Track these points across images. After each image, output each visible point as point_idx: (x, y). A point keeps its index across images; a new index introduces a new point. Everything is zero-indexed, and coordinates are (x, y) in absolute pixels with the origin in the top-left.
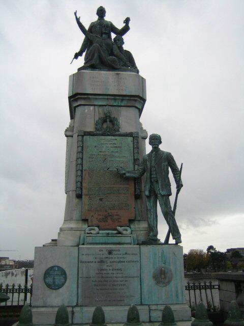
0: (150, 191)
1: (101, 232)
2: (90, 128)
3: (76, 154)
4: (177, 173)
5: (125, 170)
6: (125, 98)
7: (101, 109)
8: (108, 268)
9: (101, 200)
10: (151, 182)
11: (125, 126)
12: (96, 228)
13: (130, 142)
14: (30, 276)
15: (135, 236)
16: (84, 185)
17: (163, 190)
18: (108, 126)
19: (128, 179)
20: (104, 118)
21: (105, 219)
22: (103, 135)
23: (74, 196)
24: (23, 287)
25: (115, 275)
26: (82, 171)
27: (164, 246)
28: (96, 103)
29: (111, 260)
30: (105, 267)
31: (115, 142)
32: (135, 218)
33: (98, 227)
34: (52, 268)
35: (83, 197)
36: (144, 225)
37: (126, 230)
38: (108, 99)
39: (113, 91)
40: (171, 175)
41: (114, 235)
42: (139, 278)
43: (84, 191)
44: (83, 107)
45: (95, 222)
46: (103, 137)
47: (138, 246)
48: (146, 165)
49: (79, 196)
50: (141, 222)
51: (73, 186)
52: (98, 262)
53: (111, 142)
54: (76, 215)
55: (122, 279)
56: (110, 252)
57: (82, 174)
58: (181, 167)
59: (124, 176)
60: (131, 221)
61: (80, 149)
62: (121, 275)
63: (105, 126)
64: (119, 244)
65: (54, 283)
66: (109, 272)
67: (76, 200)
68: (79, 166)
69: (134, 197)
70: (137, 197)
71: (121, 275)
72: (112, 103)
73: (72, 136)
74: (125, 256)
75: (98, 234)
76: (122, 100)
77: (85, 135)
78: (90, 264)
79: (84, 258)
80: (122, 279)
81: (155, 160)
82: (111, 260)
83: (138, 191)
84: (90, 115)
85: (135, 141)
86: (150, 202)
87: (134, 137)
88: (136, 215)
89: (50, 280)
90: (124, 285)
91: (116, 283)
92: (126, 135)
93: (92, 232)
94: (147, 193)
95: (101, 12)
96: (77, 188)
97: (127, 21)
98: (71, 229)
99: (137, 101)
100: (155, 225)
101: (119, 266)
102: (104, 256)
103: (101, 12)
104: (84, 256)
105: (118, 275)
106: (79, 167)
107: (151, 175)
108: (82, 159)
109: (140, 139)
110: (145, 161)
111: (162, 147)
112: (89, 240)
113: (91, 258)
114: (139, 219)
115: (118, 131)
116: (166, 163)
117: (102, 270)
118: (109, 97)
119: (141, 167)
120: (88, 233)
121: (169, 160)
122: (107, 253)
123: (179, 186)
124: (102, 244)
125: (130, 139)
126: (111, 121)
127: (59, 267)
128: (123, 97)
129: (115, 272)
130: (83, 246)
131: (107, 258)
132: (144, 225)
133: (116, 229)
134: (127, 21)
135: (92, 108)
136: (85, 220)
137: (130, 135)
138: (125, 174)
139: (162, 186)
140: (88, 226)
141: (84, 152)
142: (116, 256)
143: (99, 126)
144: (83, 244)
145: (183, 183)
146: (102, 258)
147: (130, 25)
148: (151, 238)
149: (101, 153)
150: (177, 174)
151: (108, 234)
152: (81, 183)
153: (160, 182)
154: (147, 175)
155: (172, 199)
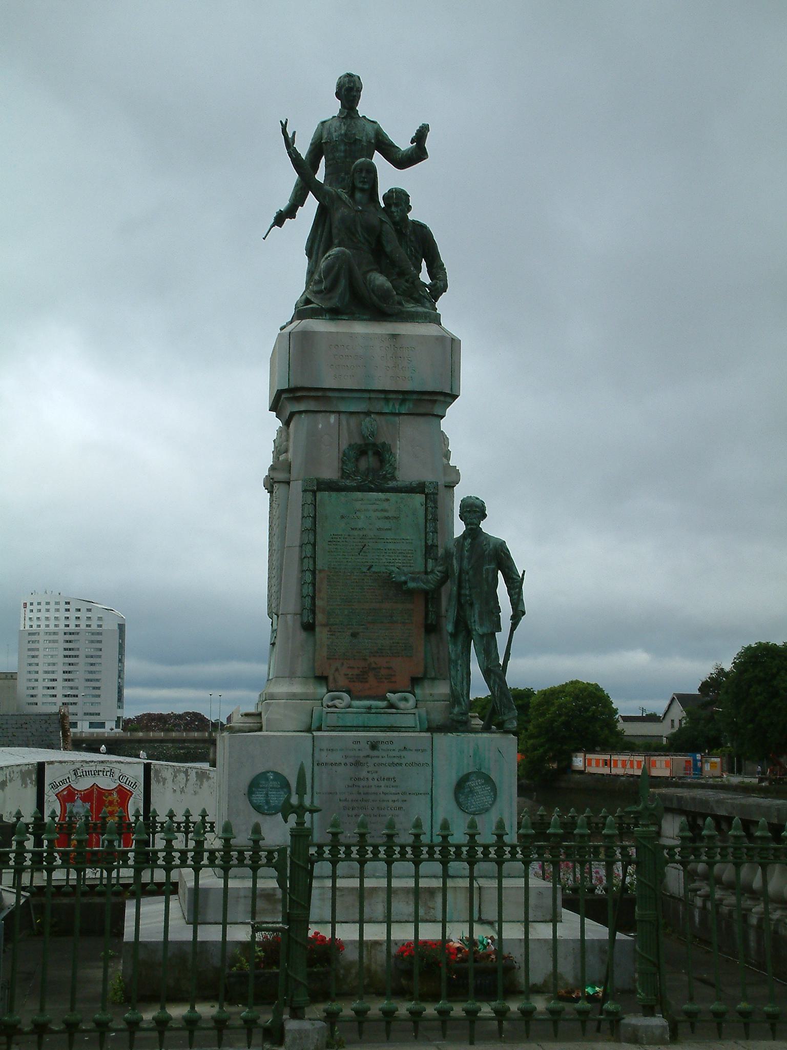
0: (457, 624)
1: (356, 703)
2: (330, 473)
3: (299, 533)
4: (515, 584)
5: (405, 575)
6: (407, 397)
7: (353, 421)
8: (370, 776)
9: (354, 635)
10: (459, 601)
11: (409, 466)
12: (345, 695)
13: (418, 506)
14: (54, 786)
15: (423, 711)
16: (318, 603)
17: (481, 625)
18: (369, 466)
19: (411, 593)
20: (361, 445)
21: (362, 677)
22: (360, 489)
23: (298, 624)
24: (28, 818)
25: (383, 789)
26: (314, 573)
27: (480, 735)
28: (342, 408)
29: (376, 760)
30: (364, 774)
31: (385, 505)
32: (425, 673)
33: (348, 692)
34: (263, 775)
35: (317, 629)
36: (442, 689)
37: (406, 699)
38: (370, 398)
39: (382, 381)
40: (502, 590)
41: (382, 711)
42: (429, 796)
43: (320, 618)
44: (311, 416)
45: (342, 682)
46: (359, 495)
47: (429, 734)
48: (452, 565)
49: (309, 628)
50: (437, 682)
51: (292, 604)
52: (351, 764)
53: (375, 507)
54: (302, 666)
55: (395, 797)
56: (374, 746)
57: (314, 578)
58: (523, 575)
59: (404, 588)
60: (415, 681)
61: (309, 522)
62: (393, 790)
63: (363, 464)
64: (392, 729)
65: (267, 802)
66: (371, 783)
67: (302, 635)
68: (306, 560)
69: (423, 630)
70: (431, 629)
71: (393, 790)
72: (379, 406)
73: (288, 483)
74: (404, 753)
75: (349, 707)
76: (403, 401)
77: (319, 489)
78: (334, 768)
79: (324, 757)
80: (395, 797)
81: (470, 558)
82: (376, 760)
83: (432, 617)
84: (332, 433)
85: (430, 504)
86: (455, 644)
87: (426, 495)
88: (426, 667)
89: (259, 798)
90: (400, 808)
91: (384, 804)
92: (411, 490)
93: (337, 702)
94: (450, 628)
95: (349, 91)
96: (303, 609)
97: (421, 136)
98: (293, 696)
99: (435, 400)
100: (465, 692)
101: (390, 772)
102: (362, 754)
103: (349, 91)
104: (324, 754)
105: (387, 790)
106: (308, 564)
107: (460, 587)
108: (314, 545)
109: (441, 489)
110: (448, 555)
111: (485, 526)
112: (332, 720)
113: (337, 757)
114: (433, 675)
115: (393, 478)
116: (493, 566)
117: (359, 779)
118: (373, 395)
119: (440, 568)
120: (328, 707)
121: (500, 557)
122: (368, 747)
123: (518, 613)
124: (357, 728)
125: (419, 498)
126: (378, 454)
127: (276, 774)
128: (404, 396)
129: (382, 783)
130: (319, 733)
131: (368, 756)
132: (442, 689)
133: (384, 698)
134: (421, 136)
135: (333, 418)
136: (322, 679)
137: (420, 488)
138: (405, 583)
139: (481, 614)
140: (329, 691)
141: (318, 530)
142: (384, 754)
143: (350, 467)
144: (319, 729)
145: (527, 608)
146: (359, 757)
147: (428, 145)
148: (455, 718)
149: (355, 533)
150: (514, 588)
151: (370, 708)
152: (313, 598)
153: (477, 606)
154: (450, 588)
155: (501, 638)
